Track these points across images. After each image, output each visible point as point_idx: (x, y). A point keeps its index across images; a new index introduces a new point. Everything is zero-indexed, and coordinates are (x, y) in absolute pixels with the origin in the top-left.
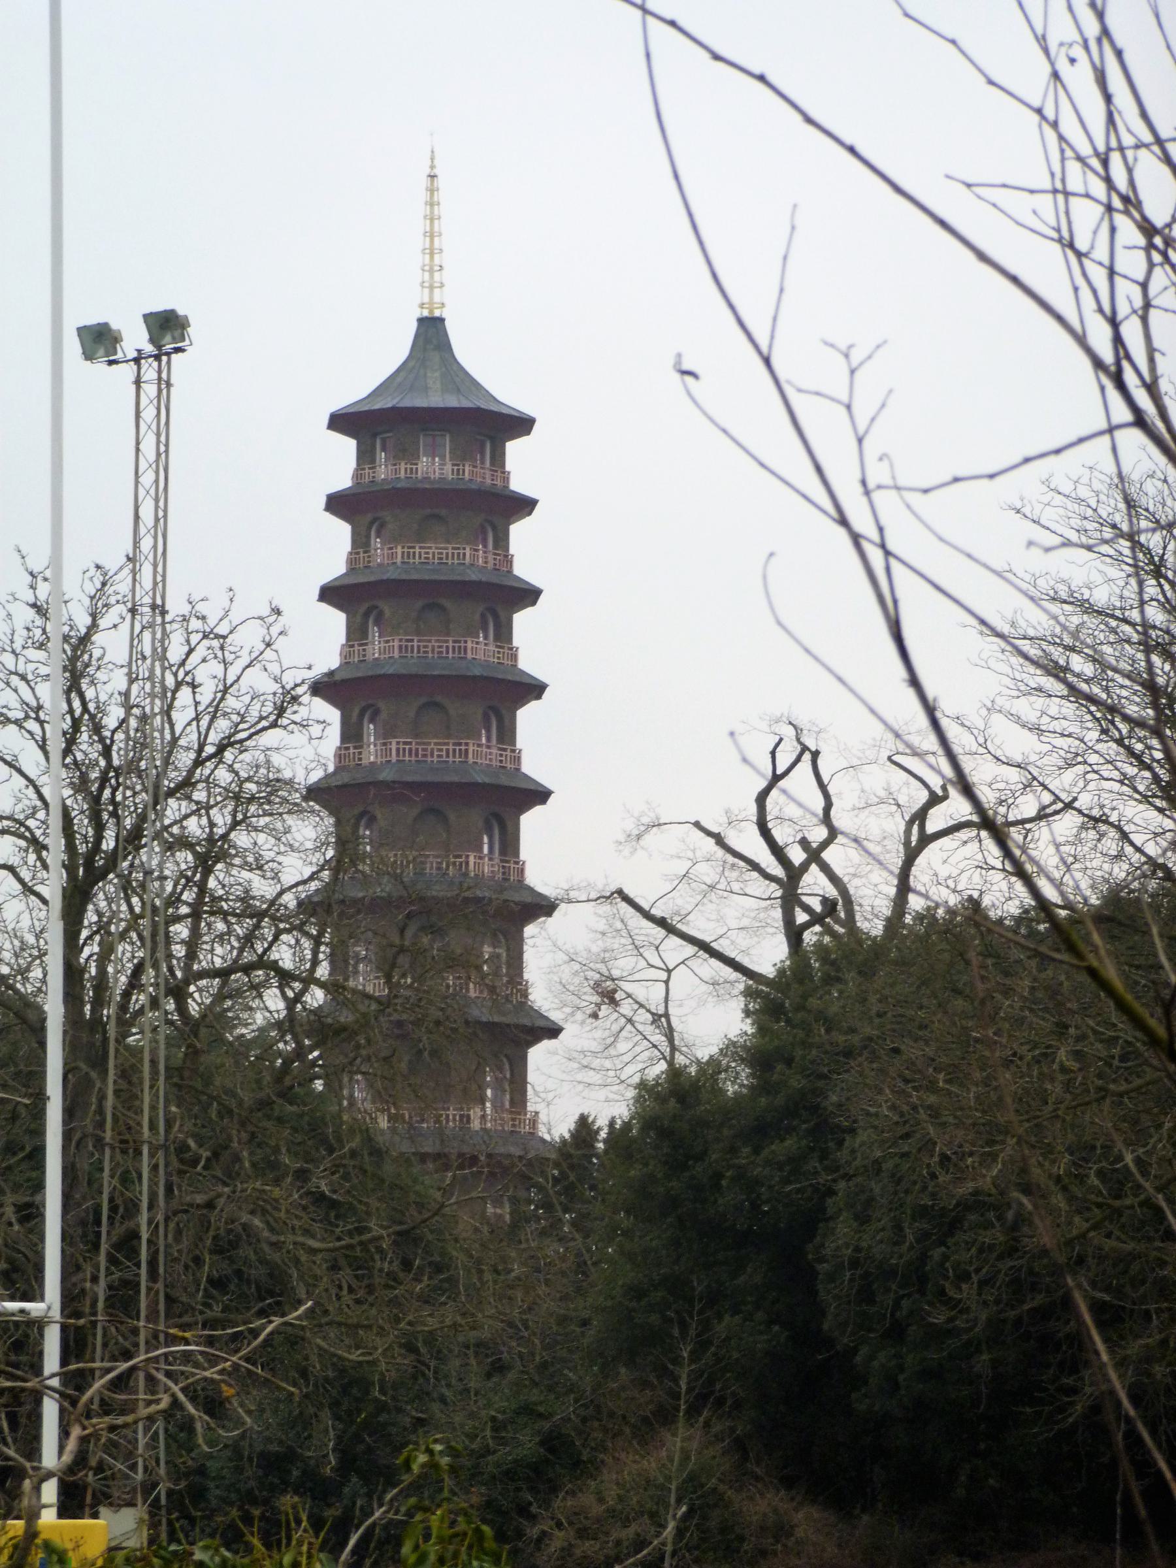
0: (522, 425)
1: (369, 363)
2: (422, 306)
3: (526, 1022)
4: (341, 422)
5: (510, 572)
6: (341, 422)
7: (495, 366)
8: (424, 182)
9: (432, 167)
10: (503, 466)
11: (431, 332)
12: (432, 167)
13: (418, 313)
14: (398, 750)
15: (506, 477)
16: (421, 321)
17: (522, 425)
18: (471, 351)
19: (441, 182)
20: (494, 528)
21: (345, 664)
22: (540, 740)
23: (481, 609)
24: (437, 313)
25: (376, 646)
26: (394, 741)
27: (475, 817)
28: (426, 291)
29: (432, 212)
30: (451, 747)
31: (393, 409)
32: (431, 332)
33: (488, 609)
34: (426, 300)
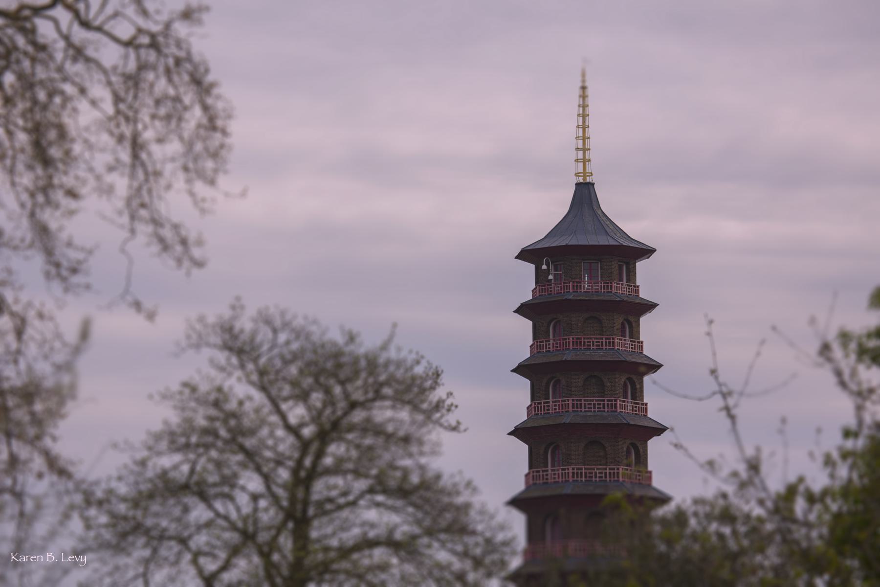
0: (646, 252)
1: (542, 211)
2: (577, 174)
3: (652, 494)
4: (525, 255)
5: (649, 485)
6: (525, 255)
7: (629, 212)
8: (577, 92)
9: (584, 81)
10: (646, 465)
11: (585, 194)
12: (584, 81)
13: (575, 180)
14: (573, 473)
15: (637, 290)
16: (576, 184)
17: (646, 252)
18: (610, 202)
19: (589, 92)
20: (627, 264)
21: (528, 487)
22: (654, 335)
23: (621, 320)
24: (588, 180)
25: (552, 472)
26: (571, 399)
27: (619, 320)
28: (581, 118)
29: (584, 110)
30: (608, 471)
31: (567, 246)
32: (585, 194)
33: (629, 379)
34: (581, 146)
